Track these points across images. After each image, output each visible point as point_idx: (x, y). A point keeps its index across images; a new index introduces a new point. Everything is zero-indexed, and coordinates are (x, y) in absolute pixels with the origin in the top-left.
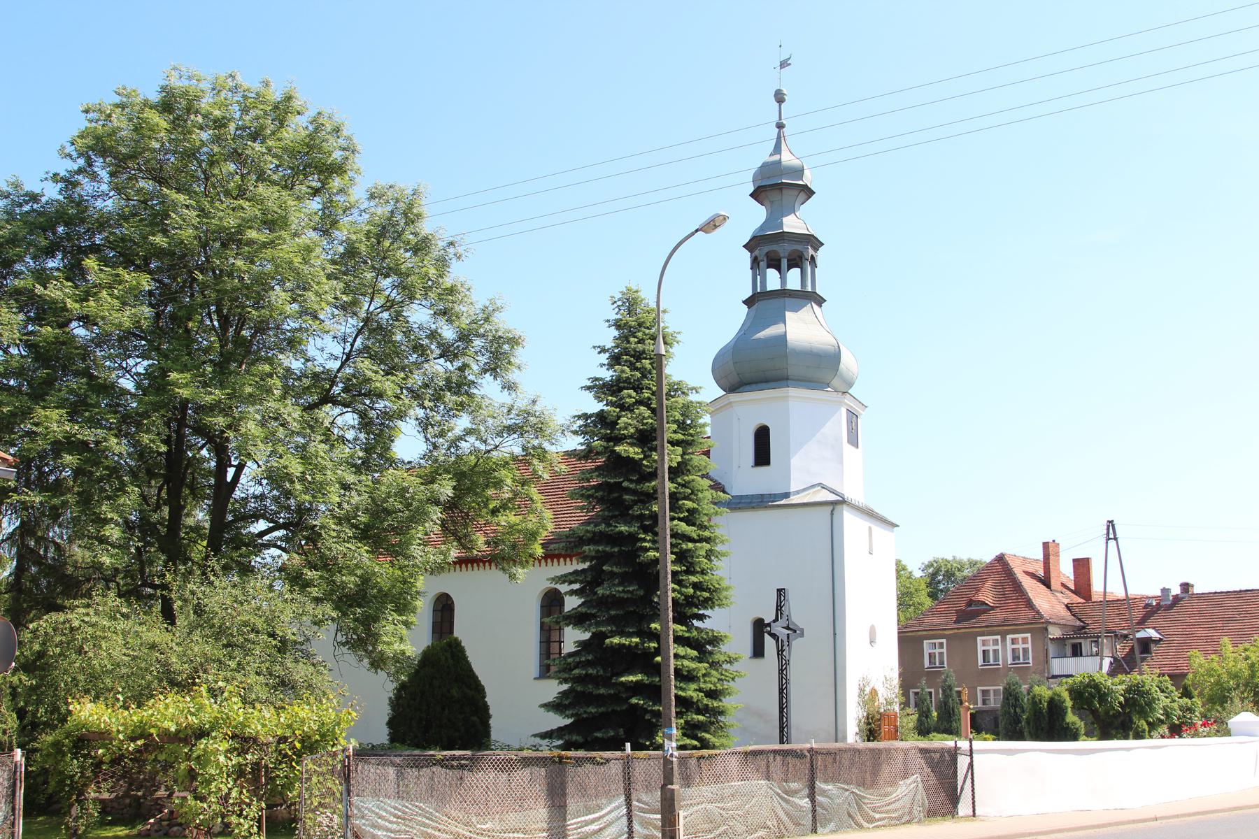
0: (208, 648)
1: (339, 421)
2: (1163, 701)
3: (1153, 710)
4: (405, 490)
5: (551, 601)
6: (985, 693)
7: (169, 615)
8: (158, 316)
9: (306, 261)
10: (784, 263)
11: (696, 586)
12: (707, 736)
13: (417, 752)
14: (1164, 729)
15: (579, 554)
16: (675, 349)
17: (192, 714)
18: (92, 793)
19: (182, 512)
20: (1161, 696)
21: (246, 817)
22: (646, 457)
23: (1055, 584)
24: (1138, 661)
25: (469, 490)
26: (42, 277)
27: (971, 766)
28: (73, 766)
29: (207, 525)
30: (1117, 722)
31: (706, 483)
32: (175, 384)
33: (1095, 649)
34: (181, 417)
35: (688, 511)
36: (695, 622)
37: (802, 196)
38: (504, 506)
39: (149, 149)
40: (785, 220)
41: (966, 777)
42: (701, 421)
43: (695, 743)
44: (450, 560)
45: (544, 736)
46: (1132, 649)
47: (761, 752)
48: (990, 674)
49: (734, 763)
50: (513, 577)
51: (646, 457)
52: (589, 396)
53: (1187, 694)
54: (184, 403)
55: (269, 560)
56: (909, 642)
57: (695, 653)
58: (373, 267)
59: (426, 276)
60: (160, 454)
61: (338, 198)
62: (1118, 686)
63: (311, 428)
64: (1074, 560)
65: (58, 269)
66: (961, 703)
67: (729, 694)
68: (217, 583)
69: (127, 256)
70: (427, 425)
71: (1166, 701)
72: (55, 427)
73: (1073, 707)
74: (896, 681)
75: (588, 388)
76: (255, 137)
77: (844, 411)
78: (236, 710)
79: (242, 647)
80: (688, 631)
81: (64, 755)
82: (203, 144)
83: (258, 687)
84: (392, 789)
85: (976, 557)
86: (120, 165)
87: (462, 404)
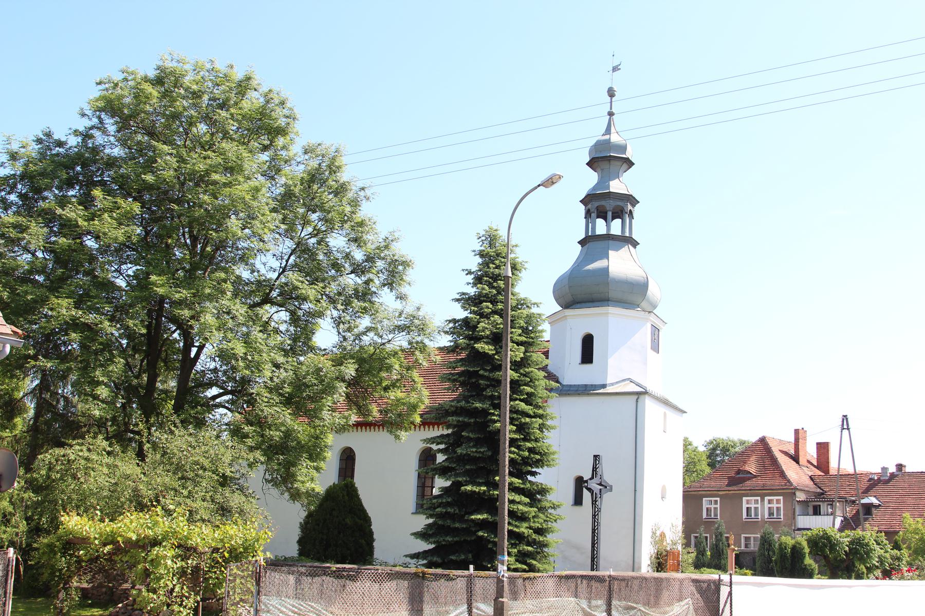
0: (167, 479)
1: (275, 317)
2: (878, 551)
3: (869, 557)
4: (320, 370)
5: (427, 457)
6: (747, 539)
7: (141, 455)
8: (147, 233)
9: (254, 198)
10: (610, 215)
11: (531, 450)
12: (534, 562)
13: (316, 564)
14: (878, 573)
15: (445, 423)
16: (523, 274)
17: (149, 528)
18: (75, 583)
19: (158, 379)
20: (877, 547)
21: (185, 607)
22: (497, 353)
23: (802, 460)
24: (862, 520)
25: (368, 372)
26: (63, 202)
27: (730, 594)
28: (62, 562)
29: (175, 390)
30: (843, 566)
31: (542, 374)
32: (154, 284)
33: (830, 510)
34: (157, 309)
35: (527, 394)
36: (529, 477)
37: (625, 166)
38: (394, 385)
39: (145, 112)
40: (612, 183)
41: (726, 602)
42: (540, 328)
43: (525, 567)
44: (351, 423)
45: (413, 556)
46: (858, 512)
47: (573, 577)
48: (752, 525)
49: (551, 584)
50: (397, 437)
51: (497, 353)
52: (458, 306)
53: (897, 546)
54: (162, 300)
55: (218, 417)
56: (691, 499)
57: (527, 500)
58: (304, 204)
59: (342, 214)
60: (142, 335)
61: (282, 152)
62: (844, 539)
63: (254, 321)
64: (818, 444)
65: (75, 196)
66: (729, 546)
67: (552, 532)
68: (177, 432)
69: (125, 188)
70: (339, 323)
71: (880, 552)
72: (64, 311)
73: (810, 553)
74: (680, 527)
75: (458, 300)
76: (223, 106)
77: (649, 326)
78: (181, 526)
79: (194, 481)
80: (523, 484)
81: (55, 554)
82: (185, 109)
83: (203, 511)
84: (291, 592)
85: (744, 438)
86: (124, 123)
87: (365, 308)
